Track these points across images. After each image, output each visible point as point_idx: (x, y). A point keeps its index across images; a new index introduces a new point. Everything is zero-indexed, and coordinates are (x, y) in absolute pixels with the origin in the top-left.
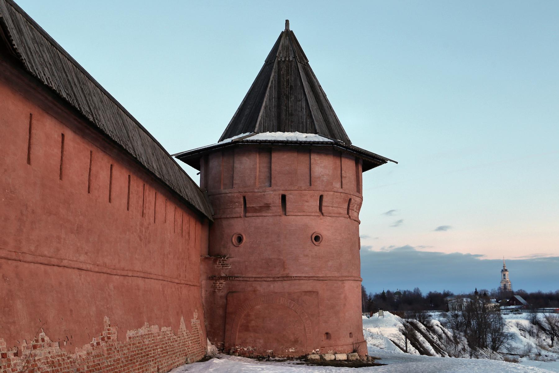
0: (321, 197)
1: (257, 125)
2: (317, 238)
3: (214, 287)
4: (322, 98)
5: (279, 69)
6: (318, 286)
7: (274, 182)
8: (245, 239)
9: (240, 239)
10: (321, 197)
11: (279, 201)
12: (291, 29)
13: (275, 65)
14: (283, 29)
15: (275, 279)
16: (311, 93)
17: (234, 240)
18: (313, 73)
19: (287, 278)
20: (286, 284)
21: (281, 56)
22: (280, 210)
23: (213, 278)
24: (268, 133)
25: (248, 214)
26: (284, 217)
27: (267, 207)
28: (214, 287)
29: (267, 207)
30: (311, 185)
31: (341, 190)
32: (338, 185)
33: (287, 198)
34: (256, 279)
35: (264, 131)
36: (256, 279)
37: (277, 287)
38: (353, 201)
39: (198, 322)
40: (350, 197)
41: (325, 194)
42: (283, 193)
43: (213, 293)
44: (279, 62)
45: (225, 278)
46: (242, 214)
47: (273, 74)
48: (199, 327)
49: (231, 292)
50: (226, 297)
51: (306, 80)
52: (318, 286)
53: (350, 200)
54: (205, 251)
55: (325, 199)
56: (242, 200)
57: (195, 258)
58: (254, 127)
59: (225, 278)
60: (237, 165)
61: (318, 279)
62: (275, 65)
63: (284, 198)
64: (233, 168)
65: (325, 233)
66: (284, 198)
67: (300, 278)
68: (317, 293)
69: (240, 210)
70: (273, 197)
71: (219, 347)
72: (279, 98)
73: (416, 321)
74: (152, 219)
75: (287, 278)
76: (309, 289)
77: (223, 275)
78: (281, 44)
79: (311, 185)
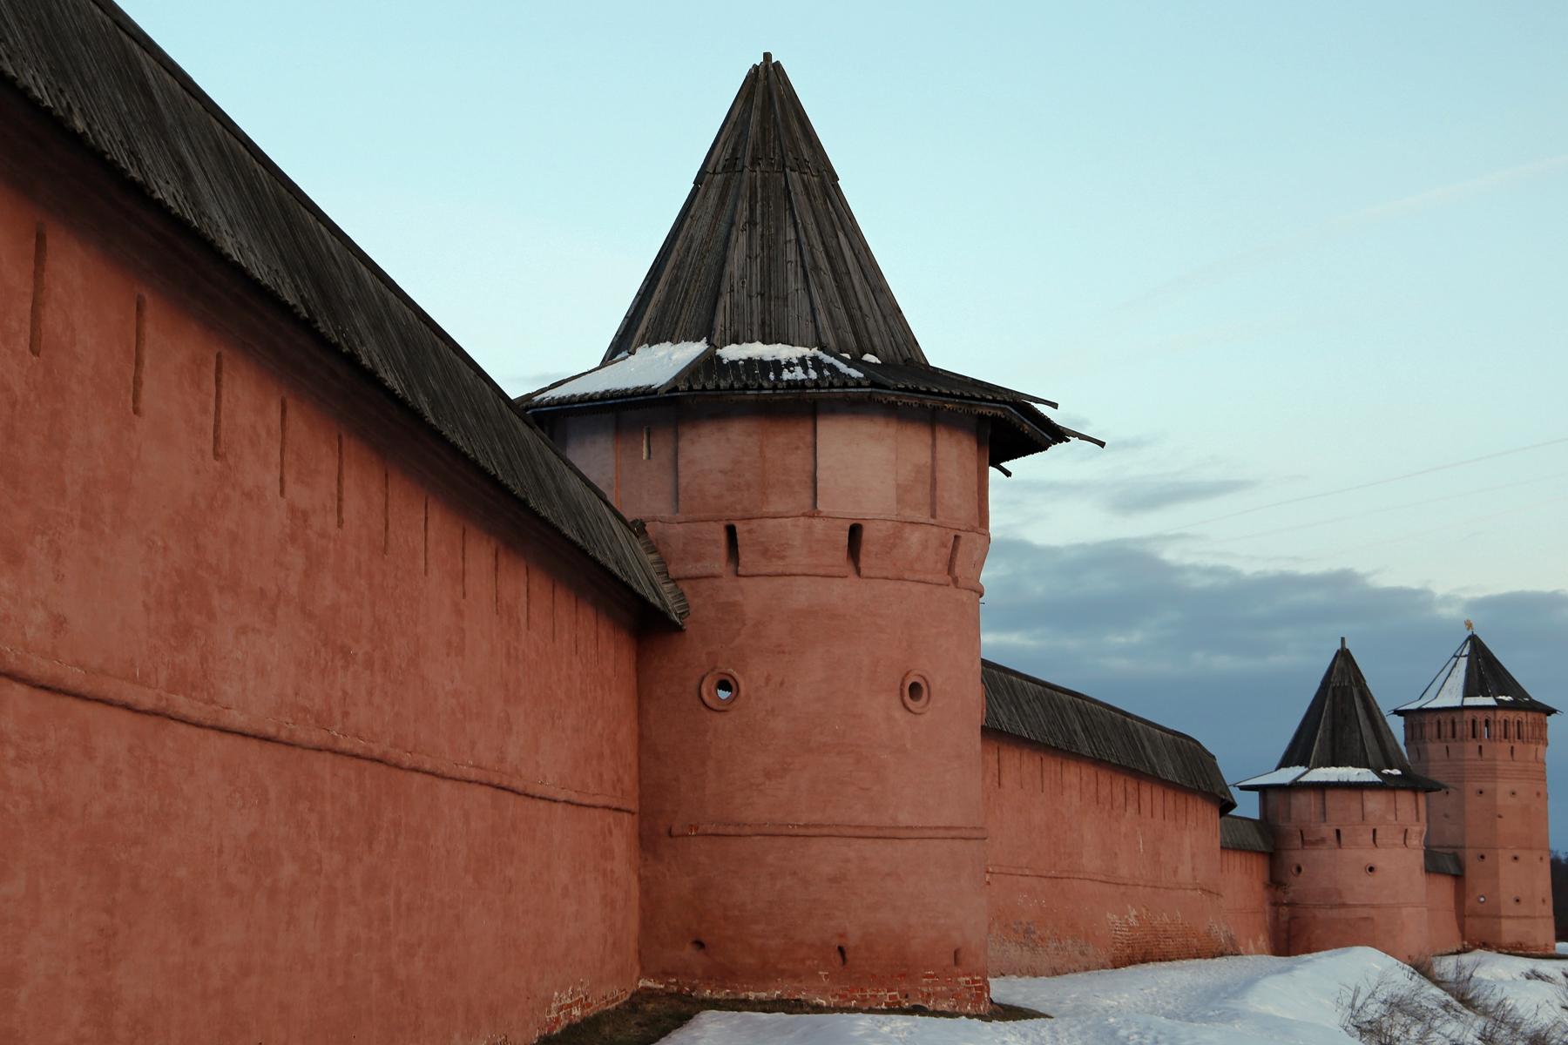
0: (1374, 831)
1: (1312, 761)
2: (1371, 869)
3: (1277, 913)
4: (1380, 722)
5: (1334, 696)
6: (1373, 913)
7: (894, 993)
8: (1303, 869)
9: (1299, 869)
10: (1374, 831)
11: (1334, 835)
12: (1347, 647)
13: (1330, 693)
14: (1339, 647)
15: (1332, 907)
16: (1367, 722)
17: (1294, 870)
18: (1370, 694)
19: (1344, 905)
20: (1343, 911)
21: (1335, 681)
22: (1335, 844)
23: (1276, 904)
24: (1322, 770)
25: (1306, 847)
26: (1339, 850)
27: (1323, 840)
28: (1277, 913)
29: (1323, 840)
30: (1363, 819)
31: (1395, 822)
32: (1392, 818)
33: (1342, 833)
34: (1315, 906)
35: (1319, 767)
36: (1315, 906)
37: (1334, 913)
38: (1409, 831)
39: (1264, 944)
40: (1405, 827)
41: (1378, 828)
42: (1337, 828)
43: (1276, 918)
44: (1334, 689)
45: (1287, 905)
46: (1300, 846)
47: (1327, 703)
48: (1265, 948)
49: (1293, 918)
50: (1289, 922)
51: (1362, 706)
52: (1373, 913)
53: (1406, 830)
54: (1266, 877)
55: (1378, 832)
56: (1299, 833)
57: (1258, 886)
58: (1309, 762)
59: (1287, 905)
60: (1293, 801)
61: (1373, 906)
62: (1330, 693)
63: (1338, 832)
64: (1290, 804)
65: (1379, 864)
66: (1338, 832)
67: (1355, 906)
68: (1372, 919)
69: (1298, 842)
70: (1327, 831)
71: (1342, 684)
72: (1333, 730)
73: (748, 380)
74: (619, 1037)
75: (1344, 905)
76: (1365, 915)
77: (1285, 902)
78: (1336, 666)
79: (1363, 819)
